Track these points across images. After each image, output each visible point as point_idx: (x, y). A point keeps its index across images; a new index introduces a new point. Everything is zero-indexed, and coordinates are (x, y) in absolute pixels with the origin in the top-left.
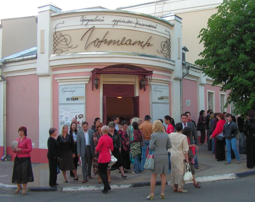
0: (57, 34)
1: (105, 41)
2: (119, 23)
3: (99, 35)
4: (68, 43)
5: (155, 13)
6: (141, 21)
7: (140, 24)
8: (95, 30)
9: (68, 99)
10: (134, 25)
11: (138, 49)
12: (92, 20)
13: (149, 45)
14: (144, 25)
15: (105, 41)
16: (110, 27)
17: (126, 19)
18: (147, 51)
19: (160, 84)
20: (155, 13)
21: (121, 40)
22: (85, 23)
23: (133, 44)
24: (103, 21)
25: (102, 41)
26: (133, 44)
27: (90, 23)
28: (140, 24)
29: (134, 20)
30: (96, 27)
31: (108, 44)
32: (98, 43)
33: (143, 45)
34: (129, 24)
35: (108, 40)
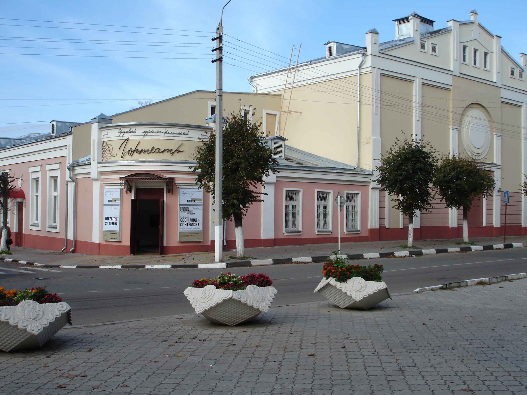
0: (105, 143)
1: (136, 151)
2: (149, 134)
3: (132, 145)
4: (111, 151)
5: (286, 84)
6: (170, 130)
7: (168, 133)
8: (129, 141)
9: (109, 201)
10: (163, 134)
11: (167, 156)
12: (127, 132)
13: (178, 151)
14: (173, 133)
15: (136, 151)
16: (141, 137)
17: (155, 130)
18: (177, 157)
19: (192, 187)
20: (286, 84)
21: (150, 150)
22: (122, 134)
23: (162, 152)
24: (135, 132)
25: (134, 151)
26: (162, 152)
27: (125, 134)
28: (168, 133)
29: (163, 130)
30: (130, 138)
31: (140, 153)
32: (131, 152)
33: (172, 152)
34: (158, 134)
35: (140, 149)
